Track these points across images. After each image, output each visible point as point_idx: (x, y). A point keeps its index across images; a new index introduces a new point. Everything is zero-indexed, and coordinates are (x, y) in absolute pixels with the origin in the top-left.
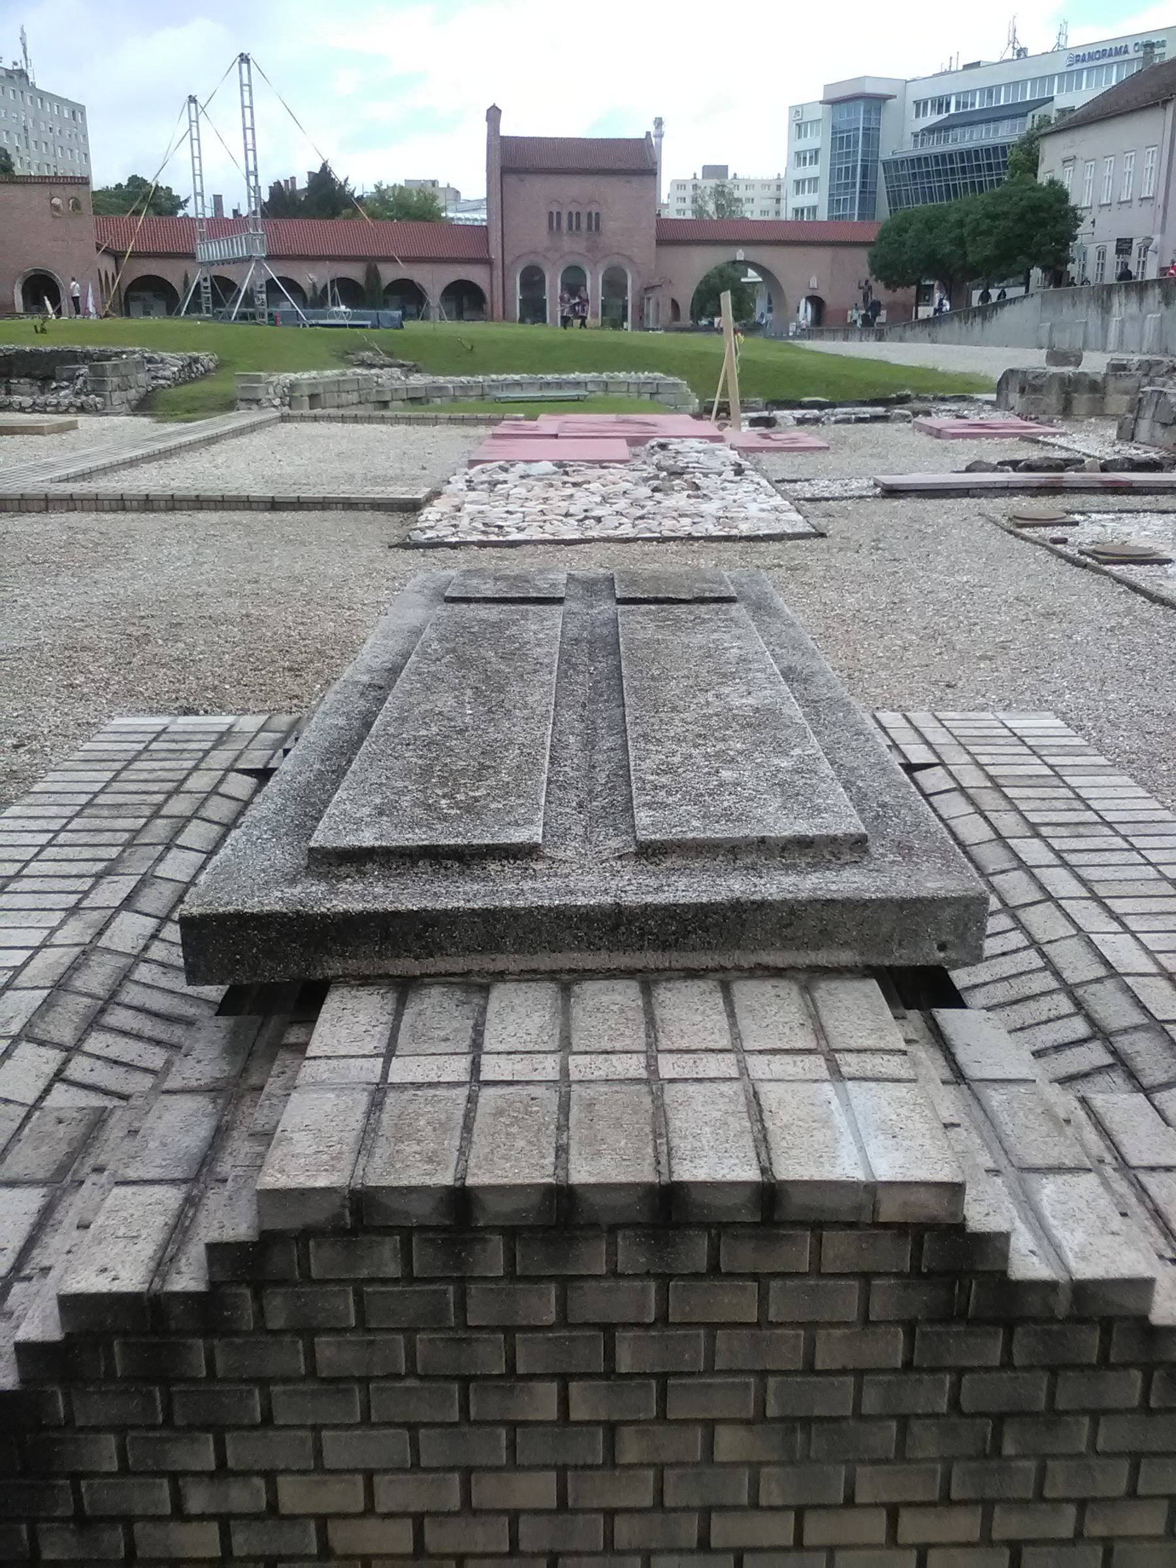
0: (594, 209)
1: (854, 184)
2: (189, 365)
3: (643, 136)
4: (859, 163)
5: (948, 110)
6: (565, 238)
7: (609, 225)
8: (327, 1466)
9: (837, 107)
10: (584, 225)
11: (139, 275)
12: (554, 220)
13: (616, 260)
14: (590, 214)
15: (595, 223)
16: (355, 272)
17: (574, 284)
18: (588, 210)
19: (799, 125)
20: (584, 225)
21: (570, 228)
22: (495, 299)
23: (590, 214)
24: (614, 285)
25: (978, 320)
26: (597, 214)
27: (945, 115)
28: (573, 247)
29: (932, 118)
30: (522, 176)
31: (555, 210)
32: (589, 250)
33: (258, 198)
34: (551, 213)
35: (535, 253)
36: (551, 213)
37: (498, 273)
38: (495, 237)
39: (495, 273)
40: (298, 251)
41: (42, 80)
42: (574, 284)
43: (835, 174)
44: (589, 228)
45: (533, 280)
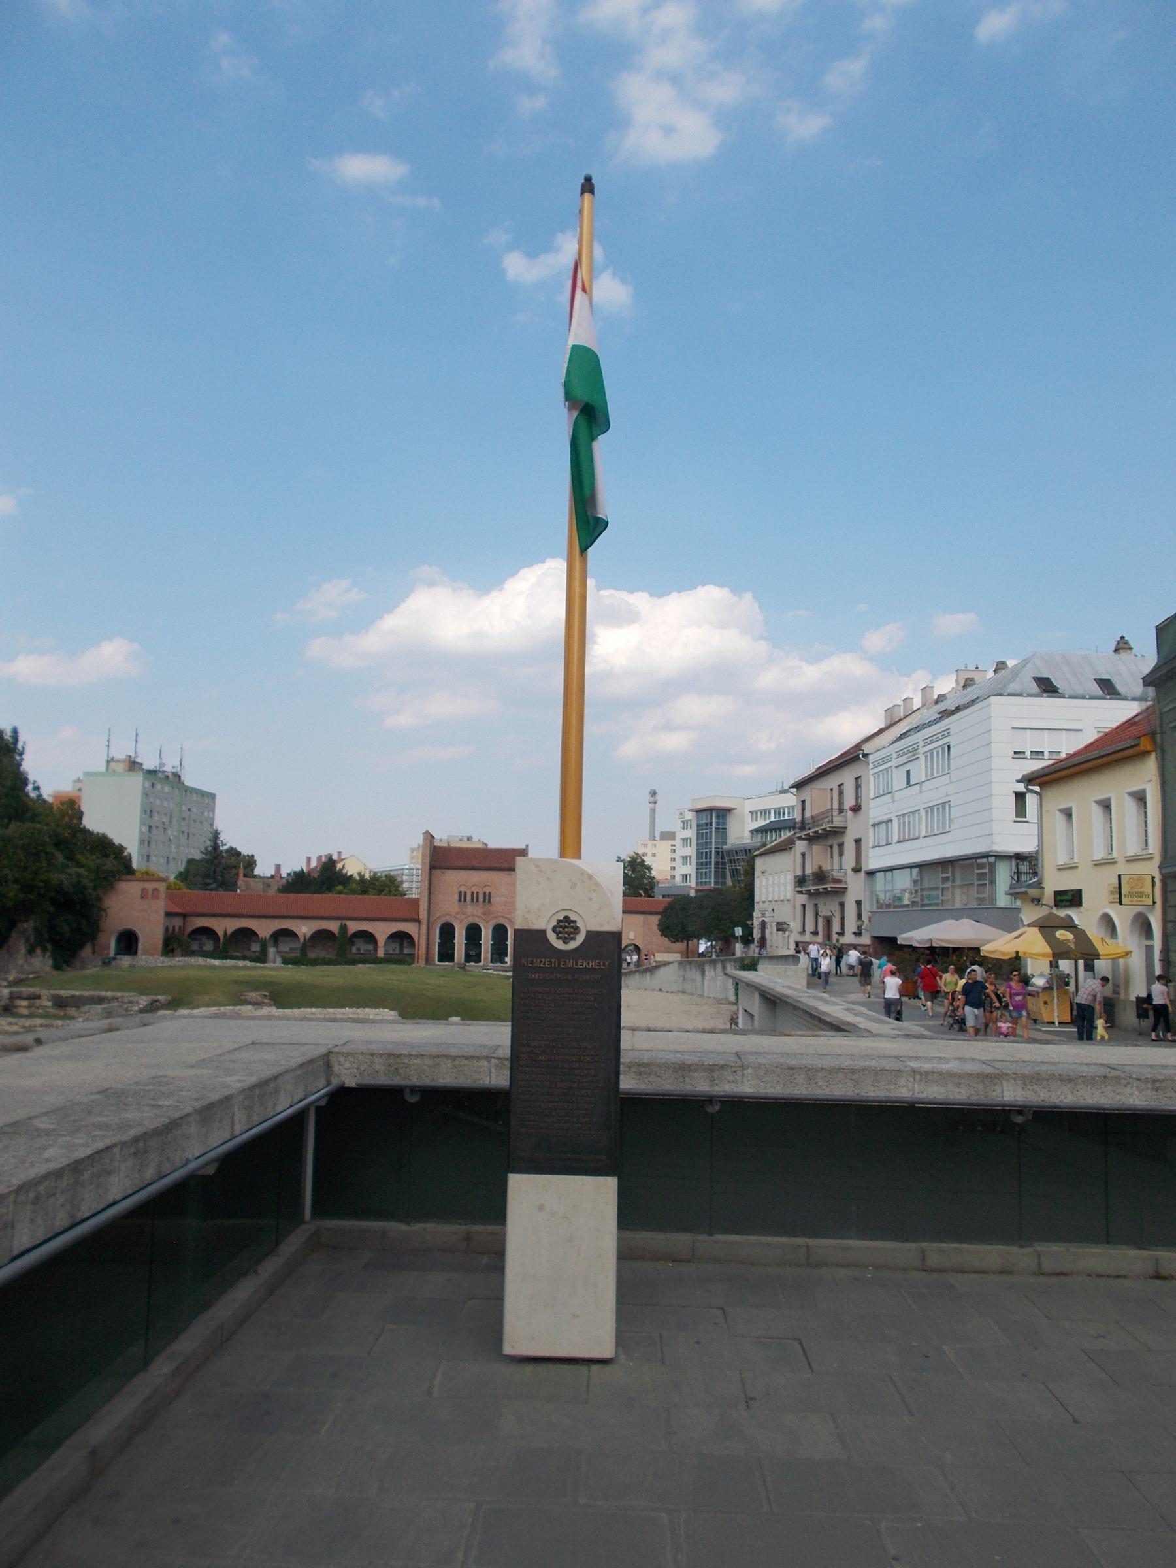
0: (487, 890)
1: (710, 863)
2: (152, 1004)
3: (524, 847)
4: (713, 849)
5: (769, 818)
6: (469, 906)
8: (508, 1350)
9: (700, 814)
10: (481, 899)
11: (198, 926)
12: (462, 897)
13: (501, 921)
14: (485, 893)
15: (488, 898)
16: (333, 926)
17: (473, 932)
18: (484, 890)
19: (683, 822)
20: (481, 899)
21: (472, 901)
22: (421, 942)
23: (485, 893)
25: (648, 974)
26: (918, 758)
27: (768, 821)
28: (473, 913)
29: (761, 823)
30: (443, 871)
31: (463, 889)
32: (484, 914)
33: (94, 946)
34: (460, 892)
35: (449, 915)
36: (460, 892)
37: (424, 927)
38: (423, 906)
39: (421, 927)
40: (295, 914)
41: (189, 780)
42: (473, 932)
43: (699, 855)
44: (484, 901)
45: (447, 931)
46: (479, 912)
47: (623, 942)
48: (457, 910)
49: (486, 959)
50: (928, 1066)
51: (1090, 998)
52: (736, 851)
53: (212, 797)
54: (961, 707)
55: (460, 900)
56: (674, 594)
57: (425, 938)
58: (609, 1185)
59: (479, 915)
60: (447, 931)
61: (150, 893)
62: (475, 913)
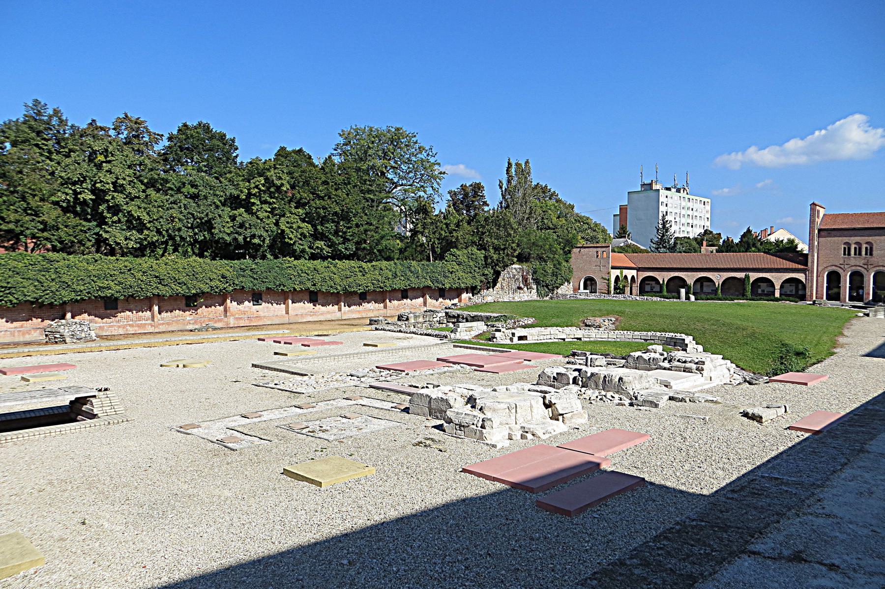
10: (863, 253)
12: (847, 252)
15: (870, 252)
17: (857, 279)
20: (863, 253)
21: (855, 254)
42: (857, 279)
49: (819, 297)
55: (845, 254)
57: (817, 284)
59: (861, 265)
60: (834, 278)
62: (858, 264)
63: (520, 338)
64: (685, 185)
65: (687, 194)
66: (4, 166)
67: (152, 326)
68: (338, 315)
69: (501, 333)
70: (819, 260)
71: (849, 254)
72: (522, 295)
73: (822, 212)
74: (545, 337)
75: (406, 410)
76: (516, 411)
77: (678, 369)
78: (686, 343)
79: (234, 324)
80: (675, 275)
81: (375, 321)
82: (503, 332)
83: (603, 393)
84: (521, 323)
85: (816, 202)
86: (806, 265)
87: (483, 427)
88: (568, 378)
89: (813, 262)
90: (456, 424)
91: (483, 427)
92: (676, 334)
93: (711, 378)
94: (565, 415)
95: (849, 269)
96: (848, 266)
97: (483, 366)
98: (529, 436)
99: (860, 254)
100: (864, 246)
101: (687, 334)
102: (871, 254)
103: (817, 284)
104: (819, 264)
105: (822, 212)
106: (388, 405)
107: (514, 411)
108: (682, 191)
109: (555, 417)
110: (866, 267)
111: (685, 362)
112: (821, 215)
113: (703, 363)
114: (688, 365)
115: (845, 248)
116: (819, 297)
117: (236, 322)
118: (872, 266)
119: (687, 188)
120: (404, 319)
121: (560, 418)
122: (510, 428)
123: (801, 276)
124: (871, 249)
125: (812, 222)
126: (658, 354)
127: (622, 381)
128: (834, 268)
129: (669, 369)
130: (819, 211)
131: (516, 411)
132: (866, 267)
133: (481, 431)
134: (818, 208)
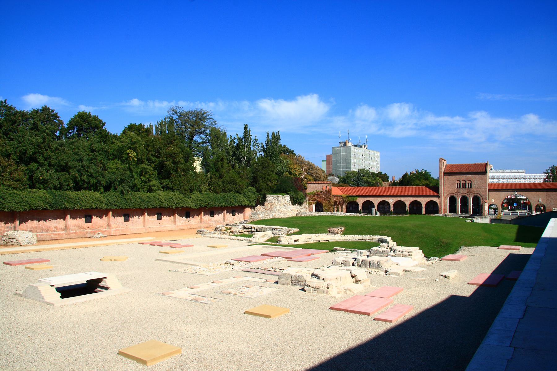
7: (474, 186)
10: (467, 186)
12: (459, 185)
15: (470, 185)
17: (464, 200)
20: (467, 186)
21: (463, 187)
24: (476, 200)
28: (464, 192)
42: (464, 200)
46: (466, 191)
47: (533, 250)
48: (456, 191)
49: (445, 211)
50: (320, 182)
51: (435, 184)
52: (385, 251)
53: (125, 221)
54: (66, 224)
55: (458, 187)
56: (37, 94)
57: (444, 203)
58: (85, 219)
59: (466, 193)
60: (453, 200)
61: (424, 206)
62: (464, 192)
63: (295, 241)
64: (365, 143)
65: (366, 149)
66: (172, 180)
67: (66, 234)
68: (173, 227)
69: (284, 238)
70: (445, 190)
71: (460, 187)
72: (280, 213)
73: (445, 163)
74: (309, 240)
75: (277, 283)
76: (340, 280)
77: (399, 256)
78: (388, 241)
79: (114, 233)
80: (367, 200)
81: (201, 231)
82: (286, 238)
83: (370, 270)
84: (291, 232)
85: (442, 158)
86: (439, 193)
87: (328, 288)
88: (350, 263)
89: (442, 191)
90: (312, 288)
91: (328, 288)
92: (382, 236)
93: (415, 259)
94: (361, 281)
95: (460, 195)
96: (459, 193)
97: (291, 258)
98: (348, 291)
99: (465, 187)
100: (467, 182)
101: (388, 236)
102: (471, 187)
103: (444, 203)
104: (445, 193)
105: (445, 163)
106: (263, 280)
107: (339, 279)
108: (363, 147)
109: (357, 282)
110: (468, 194)
111: (402, 252)
112: (445, 165)
113: (412, 252)
114: (404, 253)
115: (457, 184)
116: (445, 211)
117: (115, 232)
118: (471, 194)
119: (366, 145)
120: (219, 230)
121: (359, 282)
122: (338, 288)
123: (435, 199)
124: (471, 184)
125: (440, 169)
126: (386, 248)
127: (379, 263)
128: (452, 194)
129: (394, 256)
130: (443, 163)
131: (340, 280)
132: (468, 194)
133: (327, 290)
134: (443, 161)
